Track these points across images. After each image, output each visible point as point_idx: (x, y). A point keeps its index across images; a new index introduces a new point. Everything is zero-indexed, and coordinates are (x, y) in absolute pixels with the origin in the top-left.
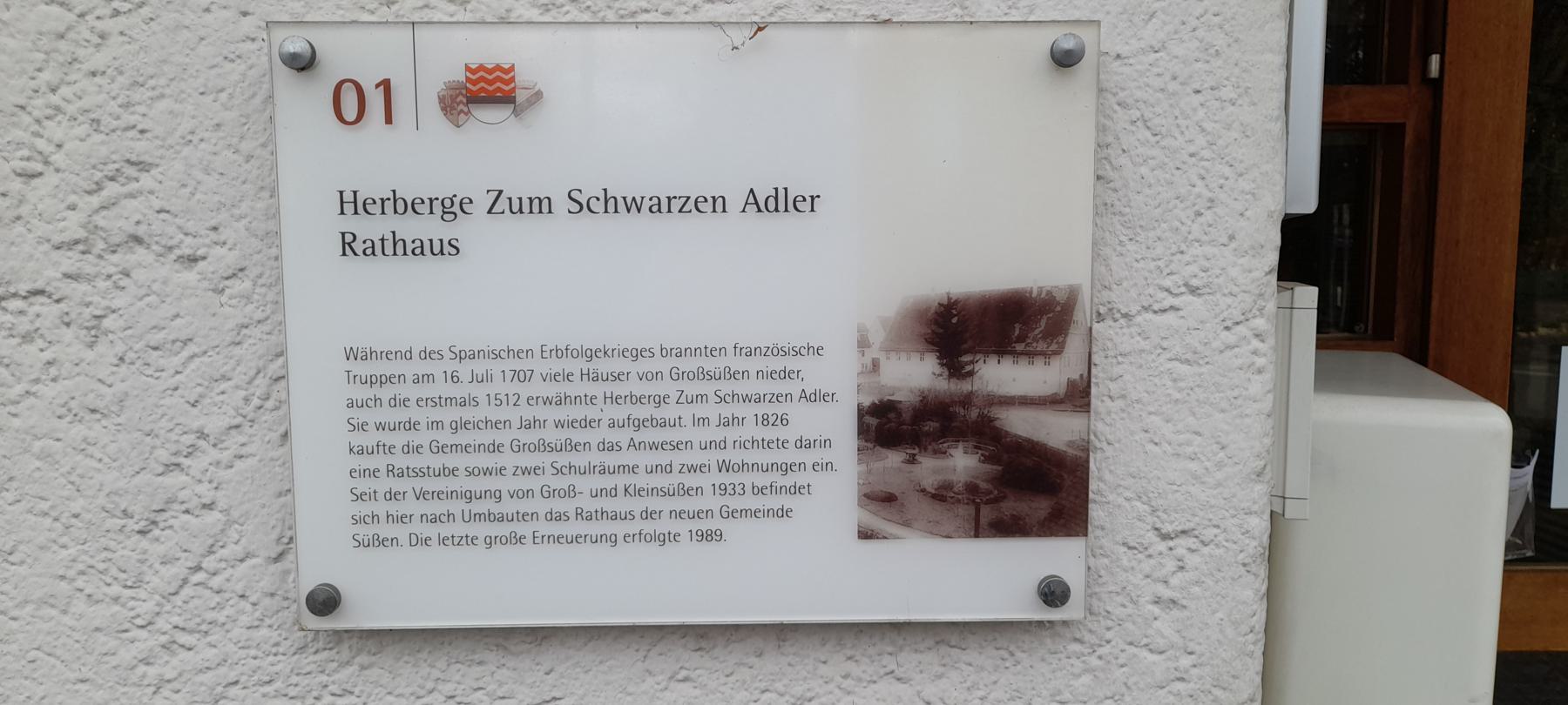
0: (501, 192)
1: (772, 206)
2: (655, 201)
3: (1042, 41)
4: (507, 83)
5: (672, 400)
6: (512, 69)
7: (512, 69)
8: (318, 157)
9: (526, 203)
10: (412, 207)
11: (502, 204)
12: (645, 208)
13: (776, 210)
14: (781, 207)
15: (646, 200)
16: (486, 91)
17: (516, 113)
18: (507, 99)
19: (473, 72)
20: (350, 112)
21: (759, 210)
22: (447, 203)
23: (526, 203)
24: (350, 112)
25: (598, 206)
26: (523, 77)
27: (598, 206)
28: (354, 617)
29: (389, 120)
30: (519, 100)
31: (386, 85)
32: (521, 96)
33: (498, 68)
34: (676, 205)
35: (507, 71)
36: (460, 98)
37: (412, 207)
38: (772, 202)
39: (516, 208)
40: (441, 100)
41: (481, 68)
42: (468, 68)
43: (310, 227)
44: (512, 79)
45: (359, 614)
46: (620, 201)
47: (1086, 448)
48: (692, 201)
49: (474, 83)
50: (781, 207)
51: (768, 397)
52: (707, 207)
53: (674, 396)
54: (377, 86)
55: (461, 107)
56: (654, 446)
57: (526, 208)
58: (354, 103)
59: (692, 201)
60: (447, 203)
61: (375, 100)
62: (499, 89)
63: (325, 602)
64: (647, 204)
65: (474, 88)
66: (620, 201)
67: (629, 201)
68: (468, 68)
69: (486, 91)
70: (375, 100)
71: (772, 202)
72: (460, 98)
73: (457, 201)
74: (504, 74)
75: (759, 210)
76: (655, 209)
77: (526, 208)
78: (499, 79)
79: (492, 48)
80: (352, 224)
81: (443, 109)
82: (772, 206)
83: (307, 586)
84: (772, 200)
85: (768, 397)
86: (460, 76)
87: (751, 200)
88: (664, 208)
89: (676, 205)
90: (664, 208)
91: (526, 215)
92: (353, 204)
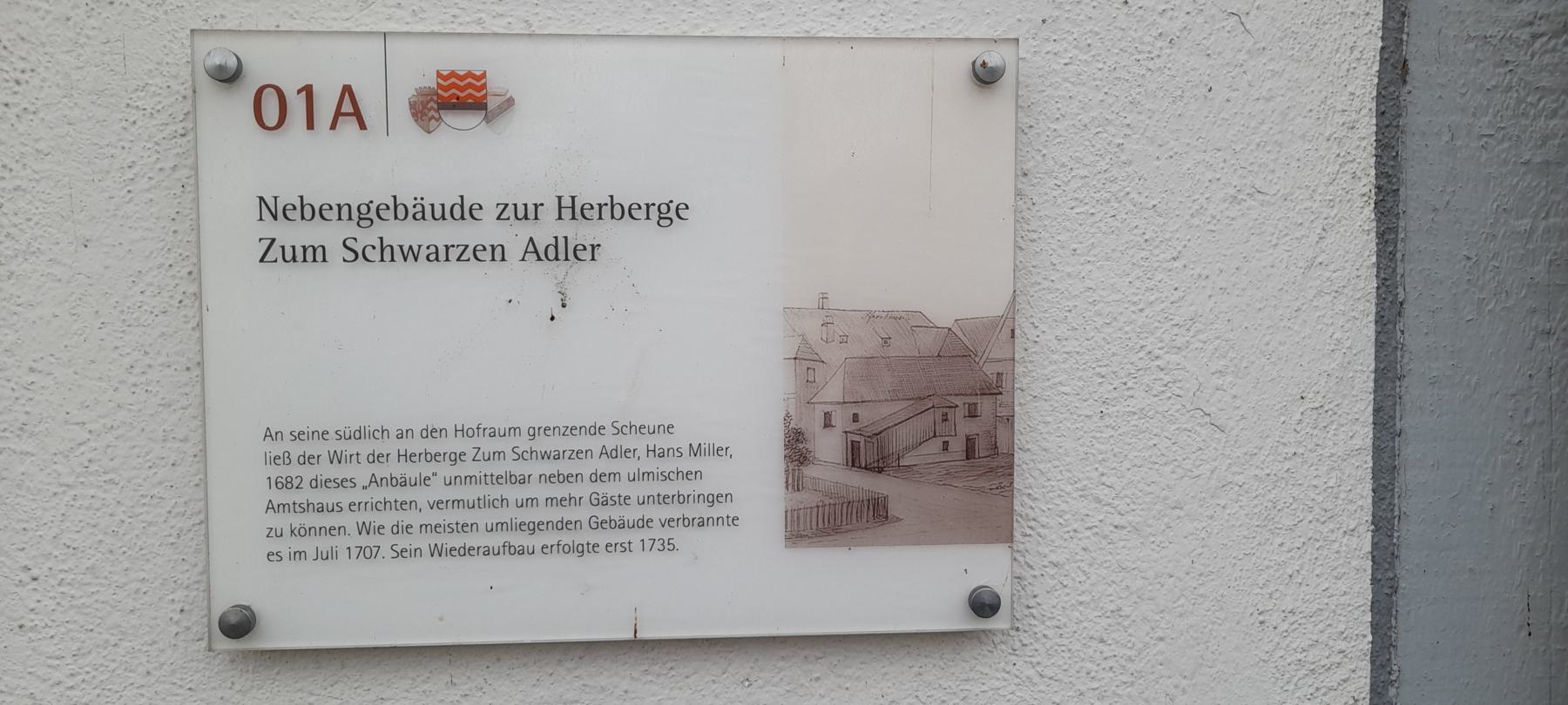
0: (273, 240)
1: (552, 255)
2: (433, 249)
3: (964, 57)
4: (480, 89)
5: (469, 458)
6: (484, 75)
7: (484, 75)
8: (244, 162)
9: (299, 252)
10: (320, 213)
11: (275, 252)
12: (422, 256)
13: (557, 259)
14: (562, 256)
15: (423, 248)
16: (458, 97)
17: (487, 119)
18: (479, 105)
19: (445, 78)
20: (271, 116)
21: (539, 259)
22: (364, 209)
23: (299, 252)
24: (271, 116)
25: (374, 255)
26: (495, 83)
27: (374, 255)
28: (273, 636)
29: (310, 126)
30: (490, 106)
31: (308, 91)
32: (492, 103)
33: (470, 74)
34: (454, 253)
35: (478, 78)
36: (432, 104)
37: (320, 213)
38: (551, 251)
39: (289, 256)
40: (412, 106)
41: (453, 74)
42: (439, 75)
43: (232, 230)
44: (484, 86)
45: (273, 636)
46: (397, 250)
47: (1006, 327)
48: (470, 250)
49: (446, 89)
50: (562, 256)
51: (567, 454)
52: (486, 256)
53: (471, 453)
54: (299, 92)
55: (432, 113)
56: (545, 456)
57: (300, 257)
58: (273, 109)
59: (470, 250)
60: (364, 209)
61: (297, 106)
62: (470, 96)
63: (239, 626)
64: (424, 253)
65: (446, 95)
66: (397, 250)
67: (406, 249)
68: (439, 75)
69: (458, 97)
70: (297, 106)
71: (551, 251)
72: (432, 104)
73: (373, 207)
74: (476, 81)
75: (539, 259)
76: (432, 257)
77: (300, 257)
78: (470, 85)
79: (460, 58)
80: (271, 229)
81: (414, 115)
82: (552, 255)
83: (221, 606)
84: (551, 249)
85: (567, 454)
86: (431, 82)
87: (531, 248)
88: (442, 256)
89: (454, 253)
90: (442, 256)
91: (300, 264)
92: (270, 209)
